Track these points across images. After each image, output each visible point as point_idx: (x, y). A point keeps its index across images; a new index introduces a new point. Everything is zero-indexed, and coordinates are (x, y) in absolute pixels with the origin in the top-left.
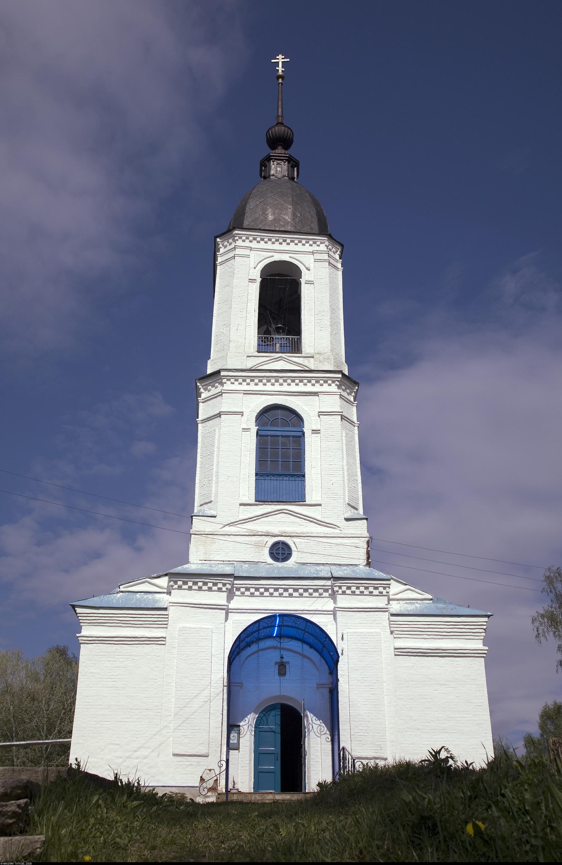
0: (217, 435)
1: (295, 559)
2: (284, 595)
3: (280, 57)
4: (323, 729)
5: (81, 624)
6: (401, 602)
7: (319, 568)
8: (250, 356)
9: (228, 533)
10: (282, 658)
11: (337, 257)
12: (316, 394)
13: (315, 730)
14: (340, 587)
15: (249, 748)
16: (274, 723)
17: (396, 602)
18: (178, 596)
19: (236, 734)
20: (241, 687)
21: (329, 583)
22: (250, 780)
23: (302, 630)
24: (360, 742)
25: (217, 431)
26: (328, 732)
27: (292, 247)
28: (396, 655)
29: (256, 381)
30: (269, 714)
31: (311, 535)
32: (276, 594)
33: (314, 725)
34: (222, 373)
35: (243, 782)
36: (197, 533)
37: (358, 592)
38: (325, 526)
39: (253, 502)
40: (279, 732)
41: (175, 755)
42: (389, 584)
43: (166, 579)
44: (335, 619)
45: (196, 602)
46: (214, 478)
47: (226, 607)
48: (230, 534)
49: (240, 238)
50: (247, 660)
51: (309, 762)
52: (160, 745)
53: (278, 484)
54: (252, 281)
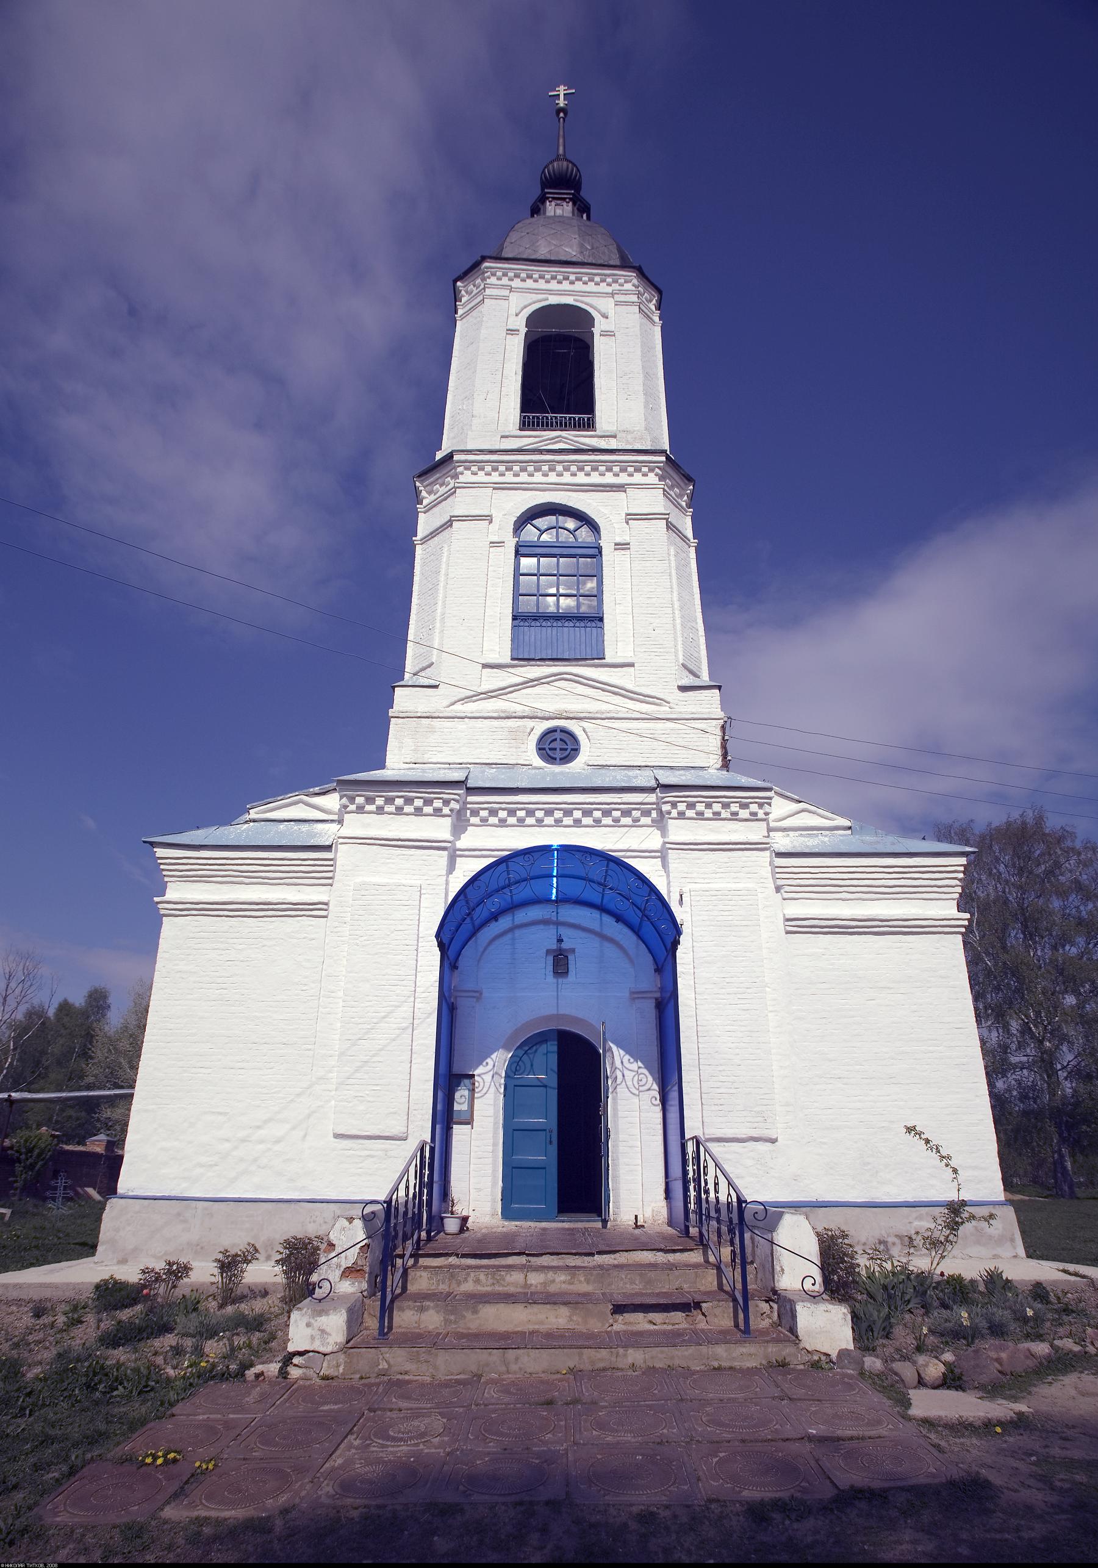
0: (445, 554)
1: (586, 758)
2: (564, 823)
3: (562, 88)
4: (644, 1080)
5: (166, 879)
6: (791, 834)
7: (631, 773)
8: (507, 437)
9: (458, 715)
10: (560, 941)
11: (653, 308)
12: (621, 488)
13: (629, 1083)
14: (674, 805)
15: (492, 1119)
16: (544, 1071)
17: (780, 834)
18: (356, 825)
19: (466, 1093)
20: (478, 999)
21: (652, 798)
22: (494, 1184)
23: (599, 884)
24: (720, 1108)
25: (445, 549)
26: (655, 1087)
27: (579, 286)
28: (788, 932)
29: (516, 468)
30: (536, 1051)
31: (616, 716)
32: (549, 820)
33: (626, 1072)
34: (456, 458)
35: (479, 1190)
36: (401, 715)
37: (708, 814)
38: (642, 702)
39: (506, 659)
40: (556, 1086)
41: (337, 1136)
42: (770, 798)
43: (336, 796)
44: (665, 865)
45: (390, 835)
46: (438, 625)
47: (449, 845)
48: (463, 715)
49: (494, 274)
50: (492, 947)
51: (615, 1146)
52: (309, 1116)
53: (554, 632)
54: (512, 332)
